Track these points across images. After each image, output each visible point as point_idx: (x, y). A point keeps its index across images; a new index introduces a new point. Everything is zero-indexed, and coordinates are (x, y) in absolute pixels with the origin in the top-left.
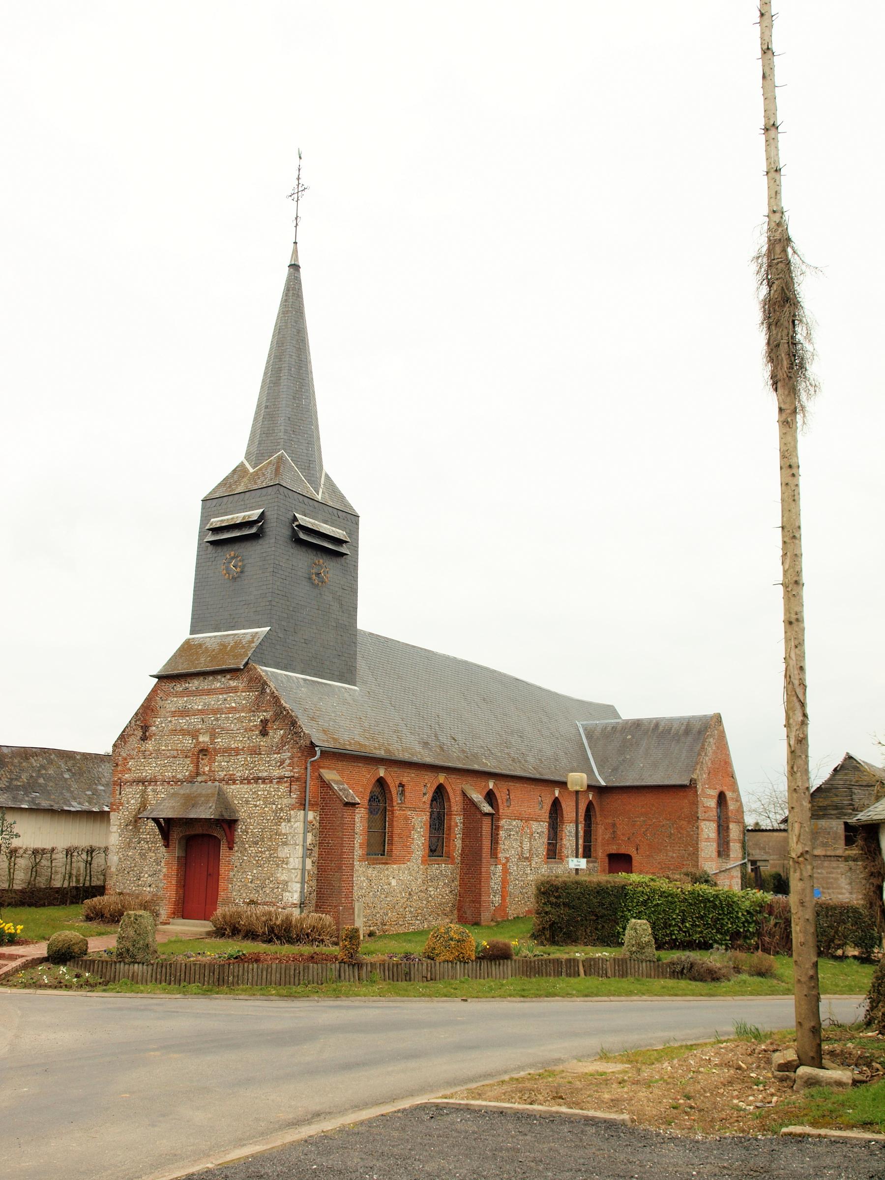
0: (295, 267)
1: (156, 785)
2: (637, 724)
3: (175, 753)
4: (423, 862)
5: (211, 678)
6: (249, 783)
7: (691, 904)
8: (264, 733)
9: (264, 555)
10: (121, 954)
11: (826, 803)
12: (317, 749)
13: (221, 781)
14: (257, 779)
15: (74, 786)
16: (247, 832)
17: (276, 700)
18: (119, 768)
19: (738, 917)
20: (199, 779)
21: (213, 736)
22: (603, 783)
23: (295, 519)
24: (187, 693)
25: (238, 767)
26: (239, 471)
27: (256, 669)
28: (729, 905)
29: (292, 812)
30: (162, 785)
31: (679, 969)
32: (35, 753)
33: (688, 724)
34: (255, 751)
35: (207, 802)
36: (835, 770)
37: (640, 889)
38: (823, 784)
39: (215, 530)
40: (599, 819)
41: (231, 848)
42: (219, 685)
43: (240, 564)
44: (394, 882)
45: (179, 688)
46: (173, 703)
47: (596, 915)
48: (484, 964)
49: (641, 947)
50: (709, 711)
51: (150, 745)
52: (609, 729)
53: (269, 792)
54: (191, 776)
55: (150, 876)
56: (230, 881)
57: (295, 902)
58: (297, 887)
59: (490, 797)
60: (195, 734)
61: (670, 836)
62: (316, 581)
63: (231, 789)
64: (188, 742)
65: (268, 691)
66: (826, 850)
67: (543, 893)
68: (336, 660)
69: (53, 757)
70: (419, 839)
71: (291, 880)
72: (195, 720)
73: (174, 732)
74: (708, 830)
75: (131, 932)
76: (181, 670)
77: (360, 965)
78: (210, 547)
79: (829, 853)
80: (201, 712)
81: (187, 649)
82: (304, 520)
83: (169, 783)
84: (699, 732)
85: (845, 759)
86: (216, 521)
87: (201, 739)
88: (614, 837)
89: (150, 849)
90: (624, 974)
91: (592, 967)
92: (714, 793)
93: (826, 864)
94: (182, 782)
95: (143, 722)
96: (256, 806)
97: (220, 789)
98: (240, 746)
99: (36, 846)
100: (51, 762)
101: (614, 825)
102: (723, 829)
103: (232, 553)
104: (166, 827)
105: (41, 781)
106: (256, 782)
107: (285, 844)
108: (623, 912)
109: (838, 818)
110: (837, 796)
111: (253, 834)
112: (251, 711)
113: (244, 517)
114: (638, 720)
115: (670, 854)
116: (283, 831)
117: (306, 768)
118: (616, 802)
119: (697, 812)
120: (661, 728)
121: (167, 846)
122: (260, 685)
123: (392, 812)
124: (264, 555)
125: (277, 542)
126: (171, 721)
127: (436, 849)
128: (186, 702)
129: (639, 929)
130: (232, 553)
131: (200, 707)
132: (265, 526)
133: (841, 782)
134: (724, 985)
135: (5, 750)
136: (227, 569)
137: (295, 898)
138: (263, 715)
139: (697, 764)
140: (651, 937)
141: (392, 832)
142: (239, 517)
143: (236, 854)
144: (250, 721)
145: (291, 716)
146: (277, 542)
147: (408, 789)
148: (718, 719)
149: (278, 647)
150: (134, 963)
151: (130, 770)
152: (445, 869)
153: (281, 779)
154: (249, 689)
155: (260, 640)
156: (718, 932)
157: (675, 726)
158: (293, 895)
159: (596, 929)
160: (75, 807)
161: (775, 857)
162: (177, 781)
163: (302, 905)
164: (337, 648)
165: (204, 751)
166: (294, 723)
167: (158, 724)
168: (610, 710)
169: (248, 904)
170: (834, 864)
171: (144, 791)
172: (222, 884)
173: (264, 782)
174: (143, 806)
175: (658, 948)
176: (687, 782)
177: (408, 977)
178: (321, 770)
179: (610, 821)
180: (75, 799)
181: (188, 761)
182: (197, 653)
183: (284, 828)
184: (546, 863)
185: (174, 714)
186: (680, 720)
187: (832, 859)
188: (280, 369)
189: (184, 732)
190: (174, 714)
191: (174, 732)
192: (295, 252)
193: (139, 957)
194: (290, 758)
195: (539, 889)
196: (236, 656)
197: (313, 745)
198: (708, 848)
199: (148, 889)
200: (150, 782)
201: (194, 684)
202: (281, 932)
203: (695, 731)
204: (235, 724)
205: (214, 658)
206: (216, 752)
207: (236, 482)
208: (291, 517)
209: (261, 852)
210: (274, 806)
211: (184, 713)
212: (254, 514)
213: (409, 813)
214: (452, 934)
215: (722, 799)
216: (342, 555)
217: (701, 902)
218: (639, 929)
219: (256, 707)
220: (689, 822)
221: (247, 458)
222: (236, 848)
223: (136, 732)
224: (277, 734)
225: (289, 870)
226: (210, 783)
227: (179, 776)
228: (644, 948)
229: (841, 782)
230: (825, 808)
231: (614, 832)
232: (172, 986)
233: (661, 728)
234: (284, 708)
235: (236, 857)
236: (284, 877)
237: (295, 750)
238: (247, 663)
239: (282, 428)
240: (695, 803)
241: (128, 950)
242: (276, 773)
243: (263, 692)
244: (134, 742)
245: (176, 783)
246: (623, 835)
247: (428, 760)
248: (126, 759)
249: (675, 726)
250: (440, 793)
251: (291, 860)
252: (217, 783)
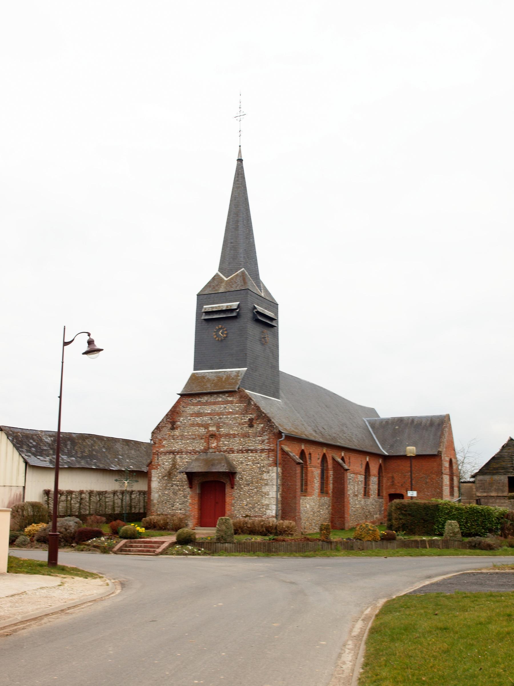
0: (240, 160)
1: (182, 454)
2: (400, 421)
3: (194, 437)
4: (319, 496)
5: (215, 396)
6: (242, 453)
7: (470, 514)
8: (251, 426)
9: (241, 328)
10: (219, 538)
11: (497, 466)
12: (283, 434)
13: (224, 451)
14: (247, 451)
15: (109, 456)
16: (242, 479)
17: (258, 408)
18: (157, 445)
19: (492, 521)
20: (211, 450)
21: (218, 427)
22: (386, 454)
23: (255, 308)
24: (199, 403)
25: (236, 444)
26: (216, 278)
27: (244, 391)
28: (489, 515)
29: (270, 468)
30: (186, 454)
31: (473, 544)
32: (86, 437)
33: (431, 421)
34: (246, 436)
35: (220, 463)
36: (503, 447)
37: (445, 506)
38: (496, 455)
39: (207, 313)
40: (384, 474)
41: (233, 488)
42: (220, 399)
43: (226, 332)
44: (308, 506)
45: (195, 401)
46: (191, 409)
47: (424, 520)
48: (385, 542)
49: (455, 534)
50: (443, 413)
51: (177, 433)
52: (384, 423)
53: (256, 458)
54: (205, 449)
55: (180, 504)
56: (233, 505)
57: (274, 515)
58: (274, 507)
59: (343, 459)
60: (206, 426)
61: (426, 483)
62: (263, 342)
63: (232, 456)
64: (202, 430)
65: (252, 403)
66: (498, 493)
67: (399, 509)
68: (272, 386)
69: (95, 439)
70: (316, 484)
71: (271, 504)
72: (206, 418)
73: (193, 425)
74: (446, 479)
75: (224, 527)
76: (196, 390)
77: (331, 543)
78: (204, 322)
79: (499, 495)
80: (210, 414)
81: (193, 379)
82: (260, 309)
83: (190, 453)
84: (439, 425)
85: (509, 441)
86: (207, 307)
87: (210, 429)
88: (393, 484)
89: (179, 490)
90: (448, 547)
91: (432, 544)
92: (448, 459)
93: (498, 501)
94: (199, 452)
95: (172, 418)
96: (247, 465)
97: (225, 457)
98: (236, 432)
99: (92, 489)
100: (95, 441)
101: (393, 477)
102: (452, 480)
103: (220, 326)
104: (191, 476)
105: (94, 453)
106: (247, 452)
107: (266, 484)
108: (437, 518)
109: (505, 474)
110: (504, 462)
111: (246, 480)
112: (242, 414)
113: (227, 306)
114: (401, 418)
115: (426, 493)
116: (265, 478)
117: (277, 445)
118: (393, 464)
119: (442, 470)
120: (415, 423)
121: (191, 487)
122: (248, 400)
123: (307, 468)
124: (241, 328)
125: (235, 320)
126: (190, 419)
127: (323, 491)
128: (200, 409)
129: (452, 526)
130: (220, 326)
131: (209, 412)
132: (240, 312)
133: (507, 454)
134: (497, 552)
135: (74, 436)
136: (218, 336)
137: (274, 513)
138: (250, 416)
139: (441, 443)
140: (459, 529)
141: (307, 479)
142: (224, 306)
143: (236, 491)
144: (242, 419)
145: (268, 417)
146: (235, 320)
147: (313, 455)
148: (448, 417)
149: (250, 379)
150: (225, 543)
151: (164, 446)
152: (326, 500)
153: (262, 451)
154: (241, 402)
155: (243, 375)
156: (483, 528)
157: (424, 421)
158: (272, 511)
159: (424, 527)
160: (114, 468)
161: (465, 498)
162: (195, 452)
163: (276, 516)
164: (272, 379)
165: (213, 436)
166: (269, 420)
167: (181, 420)
168: (372, 412)
169: (245, 517)
170: (502, 501)
171: (175, 458)
172: (227, 507)
173: (252, 452)
174: (174, 465)
175: (463, 536)
176: (436, 453)
177: (352, 548)
178: (283, 446)
179: (390, 475)
180: (112, 463)
181: (203, 441)
182: (203, 382)
183: (265, 476)
184: (364, 498)
185: (192, 415)
186: (426, 418)
187: (501, 498)
188: (237, 221)
189: (199, 425)
190: (192, 415)
191: (193, 425)
192: (240, 152)
193: (228, 540)
194: (268, 439)
195: (396, 507)
196: (231, 384)
197: (280, 433)
198: (446, 490)
199: (180, 511)
200: (178, 453)
201: (204, 399)
202: (267, 530)
203: (436, 424)
204: (232, 421)
205: (216, 385)
206: (221, 436)
207: (217, 285)
208: (252, 306)
209: (251, 489)
210: (259, 465)
211: (199, 414)
212: (234, 305)
213: (313, 469)
214: (369, 527)
215: (451, 462)
216: (273, 326)
217: (475, 513)
218: (452, 526)
219: (245, 412)
220: (437, 475)
221: (221, 269)
222: (236, 488)
223: (167, 425)
224: (259, 426)
225: (270, 498)
226: (217, 453)
227: (197, 449)
228: (456, 534)
229: (507, 454)
230: (497, 469)
231: (393, 481)
232: (242, 553)
233: (415, 423)
234: (263, 412)
235: (236, 492)
236: (266, 502)
237: (270, 435)
238: (239, 388)
239: (241, 255)
240: (441, 465)
241: (222, 536)
242: (260, 447)
243: (249, 403)
244: (166, 431)
245: (195, 453)
246: (398, 483)
247: (321, 440)
248: (161, 440)
249: (424, 421)
250: (324, 457)
251: (270, 493)
252: (222, 453)
